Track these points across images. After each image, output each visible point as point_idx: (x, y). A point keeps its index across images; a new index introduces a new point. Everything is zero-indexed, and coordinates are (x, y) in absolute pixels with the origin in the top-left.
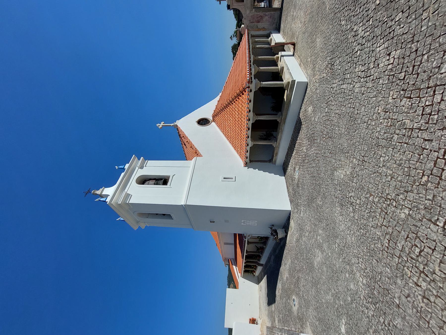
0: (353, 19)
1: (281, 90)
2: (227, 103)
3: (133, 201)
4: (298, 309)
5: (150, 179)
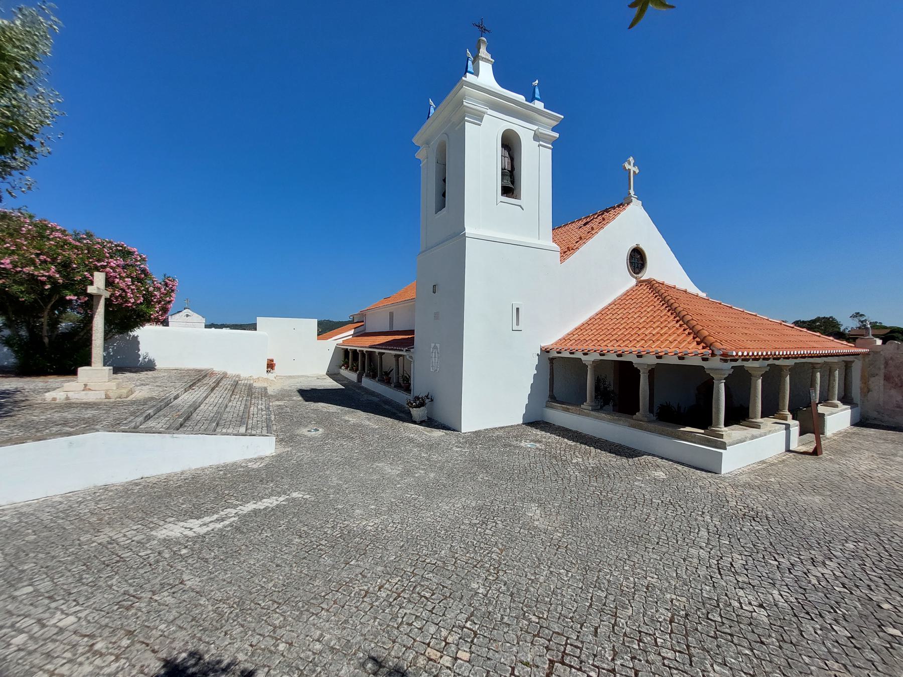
0: (855, 563)
1: (704, 419)
2: (679, 309)
3: (470, 129)
4: (305, 436)
5: (512, 159)
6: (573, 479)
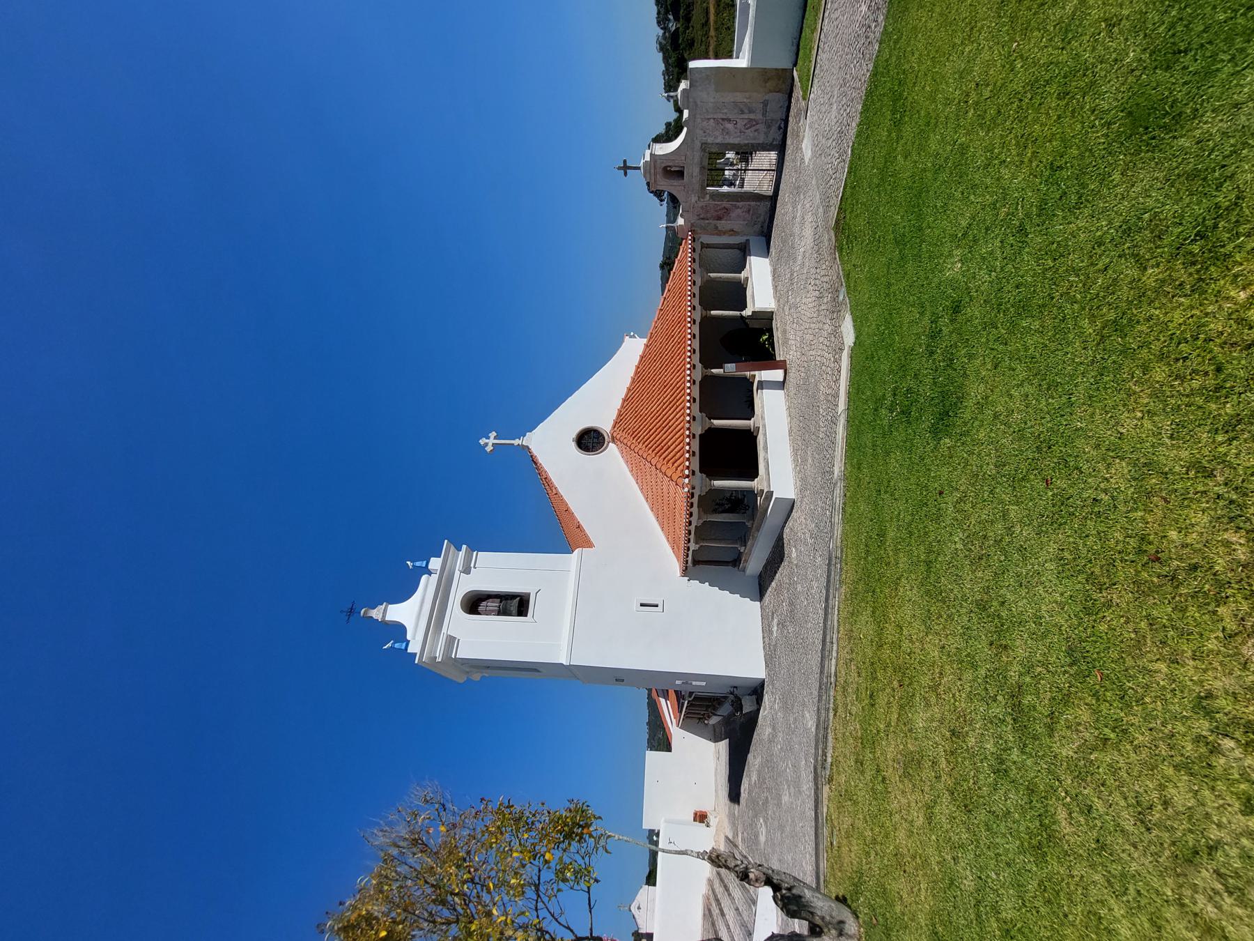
3: (463, 652)
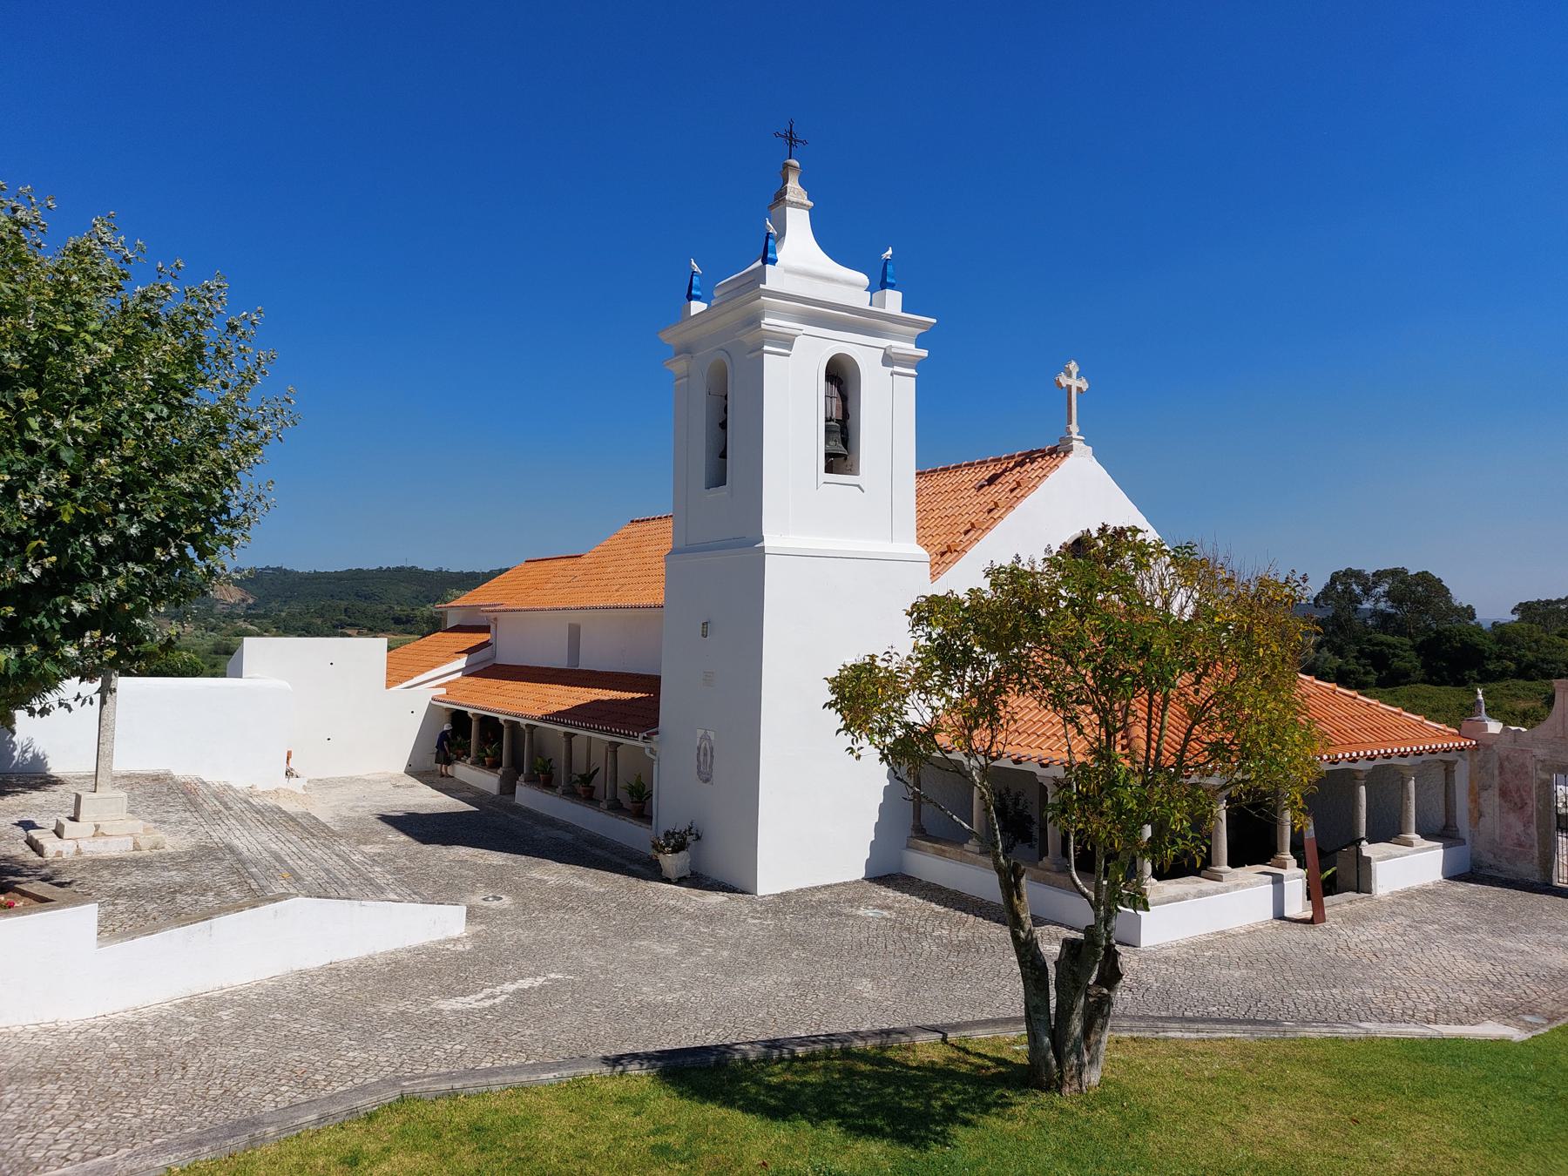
5: (844, 398)
6: (925, 955)
